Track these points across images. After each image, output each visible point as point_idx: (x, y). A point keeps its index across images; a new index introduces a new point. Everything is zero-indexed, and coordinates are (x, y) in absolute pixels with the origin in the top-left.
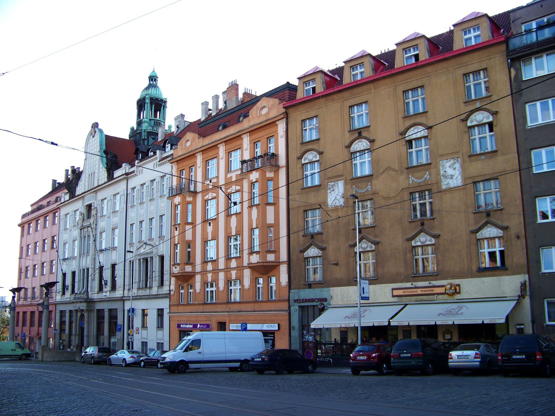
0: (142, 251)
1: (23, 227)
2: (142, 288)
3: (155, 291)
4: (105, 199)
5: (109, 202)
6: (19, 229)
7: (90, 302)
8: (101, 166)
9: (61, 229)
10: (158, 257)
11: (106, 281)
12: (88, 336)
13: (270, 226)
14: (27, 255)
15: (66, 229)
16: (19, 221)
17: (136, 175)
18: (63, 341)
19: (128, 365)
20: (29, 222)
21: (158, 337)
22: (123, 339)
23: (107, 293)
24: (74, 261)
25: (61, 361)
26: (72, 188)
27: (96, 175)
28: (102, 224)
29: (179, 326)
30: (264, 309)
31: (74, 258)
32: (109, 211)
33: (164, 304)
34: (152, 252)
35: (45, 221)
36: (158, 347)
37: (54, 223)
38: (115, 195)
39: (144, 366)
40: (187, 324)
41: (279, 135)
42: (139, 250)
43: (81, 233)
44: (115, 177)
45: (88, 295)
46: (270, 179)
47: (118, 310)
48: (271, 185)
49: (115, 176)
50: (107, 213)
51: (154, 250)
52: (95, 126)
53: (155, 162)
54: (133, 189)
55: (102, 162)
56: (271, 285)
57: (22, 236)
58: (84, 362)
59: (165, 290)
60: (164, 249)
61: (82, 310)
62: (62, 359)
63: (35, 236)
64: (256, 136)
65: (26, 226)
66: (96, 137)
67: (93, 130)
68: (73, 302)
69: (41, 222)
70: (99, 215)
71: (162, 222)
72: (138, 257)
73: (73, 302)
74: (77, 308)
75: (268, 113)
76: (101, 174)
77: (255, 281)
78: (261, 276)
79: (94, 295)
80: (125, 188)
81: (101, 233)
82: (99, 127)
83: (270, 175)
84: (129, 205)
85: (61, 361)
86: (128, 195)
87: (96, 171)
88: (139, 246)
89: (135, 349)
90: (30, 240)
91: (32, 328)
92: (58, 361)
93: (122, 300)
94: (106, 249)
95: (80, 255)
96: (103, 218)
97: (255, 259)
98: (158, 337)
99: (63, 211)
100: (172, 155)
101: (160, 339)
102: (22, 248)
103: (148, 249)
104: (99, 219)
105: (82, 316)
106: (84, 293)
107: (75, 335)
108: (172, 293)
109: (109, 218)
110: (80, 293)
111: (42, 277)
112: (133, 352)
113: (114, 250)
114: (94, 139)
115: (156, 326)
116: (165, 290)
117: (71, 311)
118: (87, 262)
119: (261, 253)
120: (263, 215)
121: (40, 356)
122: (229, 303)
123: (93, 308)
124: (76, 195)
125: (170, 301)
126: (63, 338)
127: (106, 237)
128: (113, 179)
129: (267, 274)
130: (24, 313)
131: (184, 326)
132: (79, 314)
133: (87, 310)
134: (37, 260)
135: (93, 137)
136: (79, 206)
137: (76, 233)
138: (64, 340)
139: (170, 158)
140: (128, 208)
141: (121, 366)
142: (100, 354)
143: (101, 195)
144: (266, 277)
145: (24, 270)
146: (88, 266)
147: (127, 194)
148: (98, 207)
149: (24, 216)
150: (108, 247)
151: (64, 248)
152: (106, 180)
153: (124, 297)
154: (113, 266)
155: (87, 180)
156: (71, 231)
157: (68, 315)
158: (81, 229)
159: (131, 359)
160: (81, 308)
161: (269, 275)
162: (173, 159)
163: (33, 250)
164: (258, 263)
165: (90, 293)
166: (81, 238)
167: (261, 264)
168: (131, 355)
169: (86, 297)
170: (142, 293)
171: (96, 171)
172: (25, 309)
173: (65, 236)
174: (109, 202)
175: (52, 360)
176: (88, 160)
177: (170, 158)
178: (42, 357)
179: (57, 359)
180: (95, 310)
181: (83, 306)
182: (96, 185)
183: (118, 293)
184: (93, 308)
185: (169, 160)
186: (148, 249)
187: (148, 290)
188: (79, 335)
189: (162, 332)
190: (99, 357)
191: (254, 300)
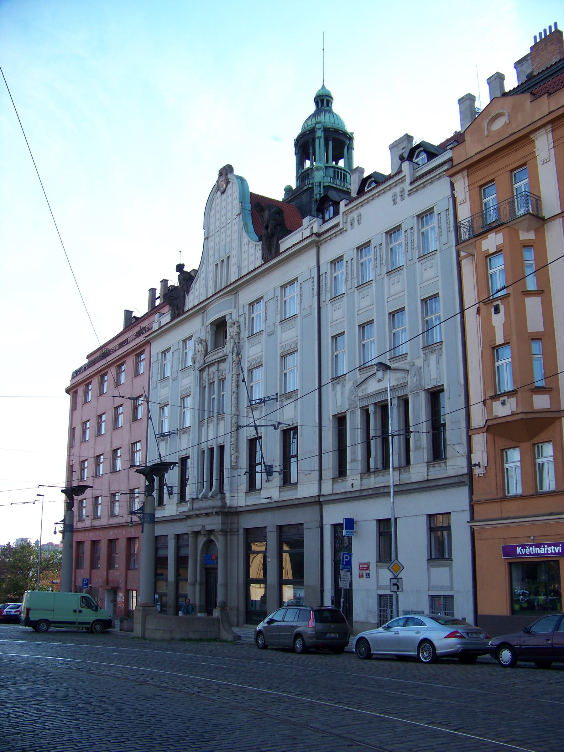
0: (373, 387)
1: (76, 392)
2: (376, 471)
3: (418, 471)
4: (169, 349)
5: (176, 354)
6: (68, 398)
7: (229, 513)
8: (246, 240)
9: (153, 380)
10: (423, 395)
11: (172, 487)
12: (226, 585)
13: (536, 337)
14: (83, 440)
15: (164, 379)
16: (68, 384)
17: (342, 231)
18: (162, 595)
19: (437, 659)
20: (87, 382)
21: (433, 583)
22: (322, 591)
23: (270, 491)
24: (185, 437)
25: (189, 640)
26: (176, 299)
27: (233, 260)
28: (252, 352)
29: (509, 551)
30: (512, 515)
31: (185, 430)
32: (175, 369)
33: (455, 502)
34: (405, 385)
35: (137, 364)
36: (432, 606)
37: (137, 374)
38: (185, 341)
39: (513, 664)
40: (539, 546)
41: (539, 160)
42: (363, 387)
43: (201, 378)
44: (281, 250)
45: (223, 499)
46: (527, 245)
47: (268, 530)
48: (529, 257)
49: (283, 248)
50: (172, 372)
51: (411, 380)
52: (226, 171)
53: (397, 190)
54: (335, 262)
55: (247, 232)
56: (540, 461)
57: (73, 408)
58: (265, 647)
59: (455, 464)
60: (439, 370)
61: (211, 532)
62: (191, 635)
63: (96, 404)
64: (483, 174)
65: (81, 391)
66: (229, 191)
67: (223, 178)
68: (188, 517)
69: (109, 378)
70: (245, 334)
71: (336, 350)
72: (360, 404)
73: (188, 517)
74: (198, 529)
75: (506, 125)
76: (245, 256)
77: (498, 458)
78: (515, 444)
79: (239, 498)
80: (315, 263)
81: (250, 371)
82: (236, 172)
83: (527, 236)
84: (326, 296)
85: (189, 640)
86: (323, 278)
87: (234, 253)
88: (359, 377)
89: (458, 615)
90: (88, 412)
91: (93, 571)
92: (182, 640)
93: (318, 502)
94: (170, 433)
95: (201, 422)
96: (337, 304)
97: (503, 410)
98: (433, 583)
99: (157, 347)
100: (451, 160)
101: (442, 588)
102: (72, 430)
103: (389, 380)
104: (246, 344)
105: (209, 543)
106: (213, 496)
107: (194, 584)
108: (477, 471)
109: (271, 334)
110: (205, 497)
111: (114, 476)
112: (455, 622)
113: (184, 433)
114: (224, 196)
115: (424, 554)
116: (455, 464)
117: (178, 537)
118: (217, 433)
119: (519, 394)
120: (519, 317)
121: (138, 628)
122: (505, 499)
123: (235, 526)
124: (281, 251)
125: (471, 492)
126: (159, 591)
127: (171, 413)
128: (278, 253)
129: (531, 438)
130: (95, 543)
131: (527, 550)
132: (202, 540)
133: (222, 530)
134: (104, 447)
135: (223, 192)
136: (197, 328)
137: (189, 381)
138: (165, 595)
139: (445, 167)
140: (322, 304)
141: (416, 659)
142: (320, 626)
143: (246, 296)
144: (527, 445)
145: (77, 468)
146: (220, 441)
147: (319, 276)
148: (242, 320)
149: (76, 374)
150: (173, 429)
151: (161, 415)
152: (259, 262)
153: (319, 496)
154: (435, 396)
155: (211, 275)
156: (175, 379)
157: (172, 544)
158: (201, 371)
159: (453, 640)
160: (208, 528)
161: (535, 440)
162: (453, 166)
163: (94, 431)
164: (513, 414)
165: (228, 494)
166: (203, 388)
167: (521, 416)
168: (448, 630)
169: (219, 503)
170: (373, 482)
171: (234, 253)
172: (112, 534)
173: (161, 393)
174: (176, 354)
175: (167, 636)
176: (211, 239)
177: (445, 167)
178: (144, 629)
179: (178, 635)
180: (241, 531)
181: (214, 523)
182: (233, 278)
183: (307, 489)
184: (235, 526)
185: (446, 171)
186: (389, 380)
187: (373, 476)
188: (201, 584)
189: (446, 570)
190: (319, 634)
191: (500, 495)
